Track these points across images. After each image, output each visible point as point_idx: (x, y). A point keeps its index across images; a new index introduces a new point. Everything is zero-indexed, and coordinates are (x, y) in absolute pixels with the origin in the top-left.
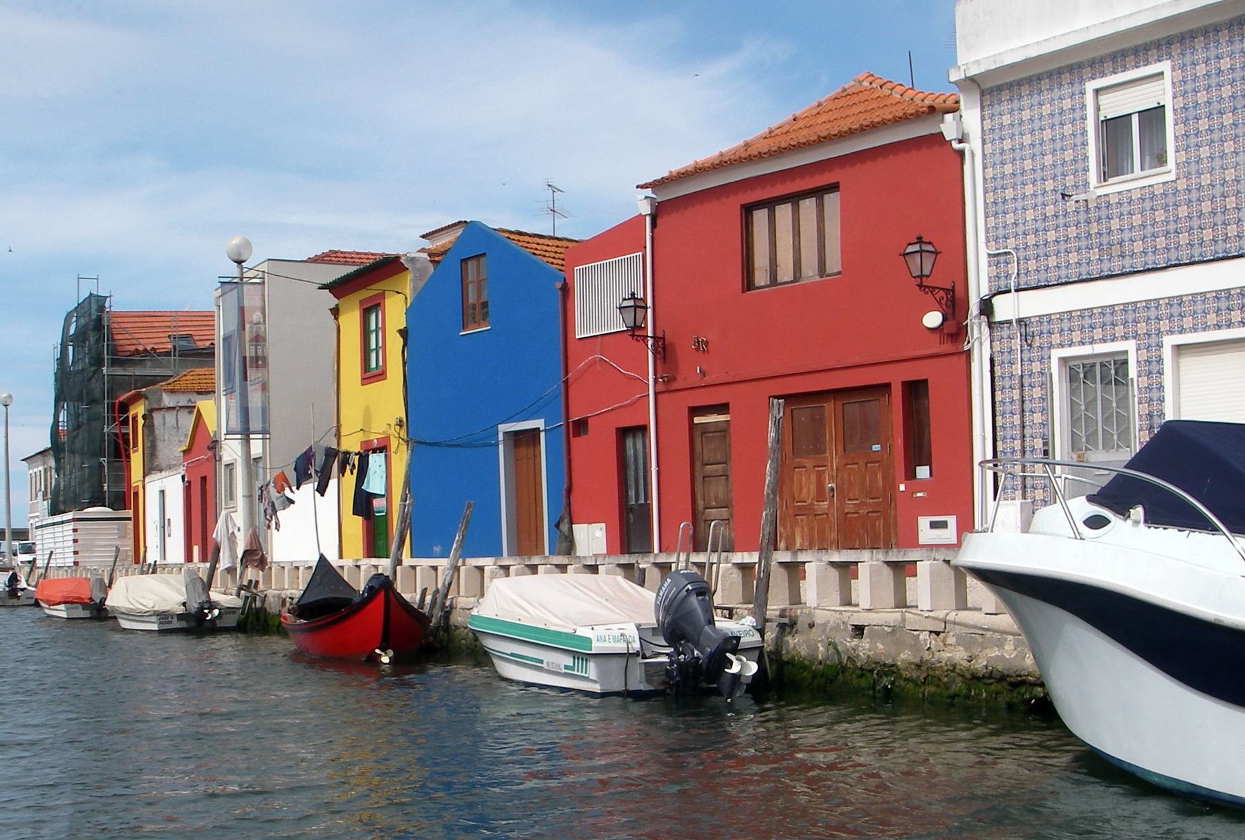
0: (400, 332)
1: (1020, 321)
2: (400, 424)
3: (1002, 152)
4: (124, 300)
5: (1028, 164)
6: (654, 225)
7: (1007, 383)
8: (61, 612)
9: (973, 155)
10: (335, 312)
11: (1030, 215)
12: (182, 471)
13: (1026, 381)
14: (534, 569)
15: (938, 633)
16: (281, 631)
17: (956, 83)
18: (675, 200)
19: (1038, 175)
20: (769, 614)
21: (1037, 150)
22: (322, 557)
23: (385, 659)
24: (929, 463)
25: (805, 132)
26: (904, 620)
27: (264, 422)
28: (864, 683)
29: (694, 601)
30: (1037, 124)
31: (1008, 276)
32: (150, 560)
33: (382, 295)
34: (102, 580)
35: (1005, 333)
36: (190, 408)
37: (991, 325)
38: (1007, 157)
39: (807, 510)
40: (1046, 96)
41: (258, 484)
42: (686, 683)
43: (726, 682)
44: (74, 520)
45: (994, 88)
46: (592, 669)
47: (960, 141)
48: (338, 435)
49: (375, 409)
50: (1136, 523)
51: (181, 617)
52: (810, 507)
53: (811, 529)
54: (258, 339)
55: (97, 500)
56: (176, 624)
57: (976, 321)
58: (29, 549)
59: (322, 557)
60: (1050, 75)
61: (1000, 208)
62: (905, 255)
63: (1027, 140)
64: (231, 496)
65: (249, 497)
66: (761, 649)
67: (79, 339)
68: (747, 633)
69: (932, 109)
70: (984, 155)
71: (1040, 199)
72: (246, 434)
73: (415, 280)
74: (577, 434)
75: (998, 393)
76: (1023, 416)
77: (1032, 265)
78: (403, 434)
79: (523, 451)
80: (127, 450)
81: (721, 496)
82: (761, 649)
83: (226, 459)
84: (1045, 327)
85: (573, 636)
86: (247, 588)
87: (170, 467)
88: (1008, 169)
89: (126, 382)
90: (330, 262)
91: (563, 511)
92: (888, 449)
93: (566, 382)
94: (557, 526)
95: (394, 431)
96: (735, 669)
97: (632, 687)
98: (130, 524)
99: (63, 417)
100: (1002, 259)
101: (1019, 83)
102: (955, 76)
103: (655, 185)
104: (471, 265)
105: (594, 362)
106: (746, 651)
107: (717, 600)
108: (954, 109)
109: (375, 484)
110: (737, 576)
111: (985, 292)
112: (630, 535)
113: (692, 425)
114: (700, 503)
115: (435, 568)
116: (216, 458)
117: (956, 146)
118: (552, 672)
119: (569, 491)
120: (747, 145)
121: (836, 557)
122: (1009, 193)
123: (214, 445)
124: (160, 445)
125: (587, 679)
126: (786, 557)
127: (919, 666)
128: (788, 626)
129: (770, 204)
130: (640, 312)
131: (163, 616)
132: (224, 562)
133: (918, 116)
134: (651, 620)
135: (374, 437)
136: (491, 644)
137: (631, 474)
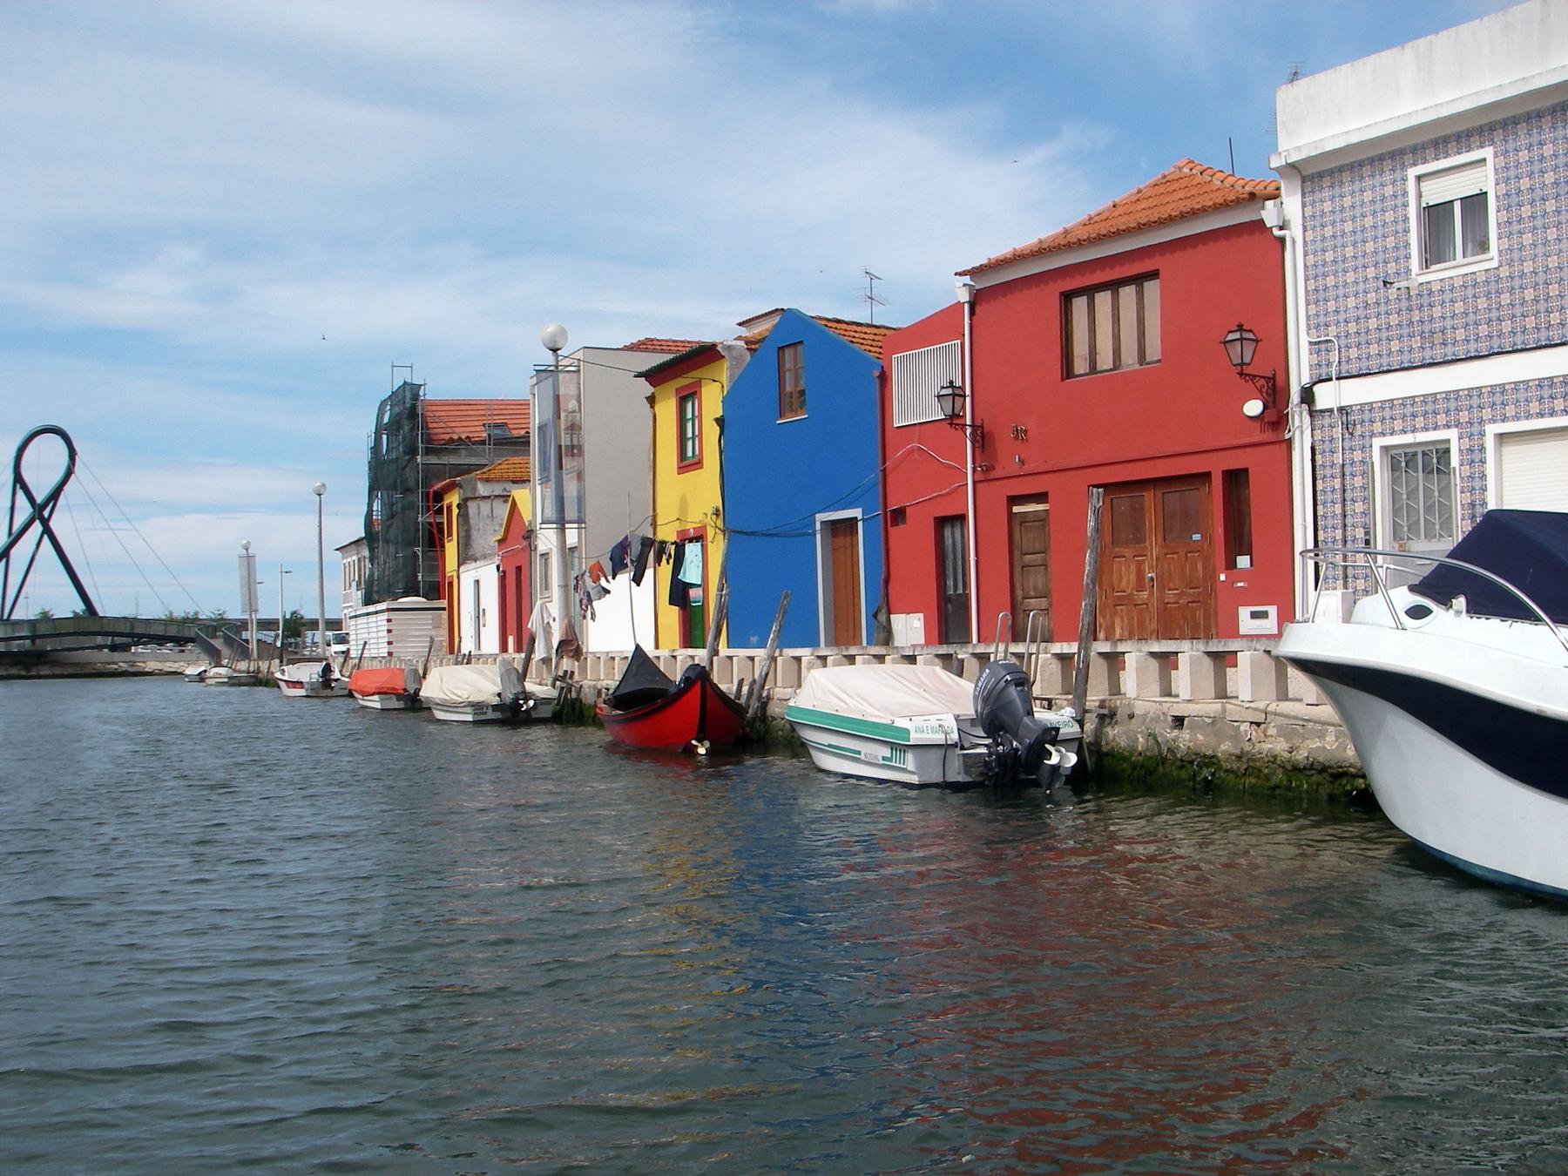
0: (718, 421)
1: (1341, 409)
2: (717, 513)
3: (1324, 239)
4: (441, 387)
5: (1349, 251)
6: (972, 313)
7: (1328, 472)
8: (375, 702)
9: (1294, 242)
10: (651, 400)
11: (1351, 302)
12: (497, 561)
13: (1348, 470)
14: (851, 659)
15: (1258, 724)
16: (597, 722)
17: (1277, 170)
18: (993, 288)
19: (1360, 262)
22: (638, 648)
23: (702, 751)
25: (1124, 219)
26: (1224, 711)
27: (579, 511)
30: (1358, 211)
31: (1329, 364)
32: (465, 651)
33: (698, 384)
34: (416, 671)
35: (1327, 421)
36: (505, 498)
37: (1312, 413)
38: (1329, 244)
39: (1126, 600)
41: (574, 574)
42: (1005, 774)
43: (1045, 772)
44: (388, 610)
45: (1315, 174)
46: (910, 761)
47: (1281, 228)
48: (654, 524)
50: (1459, 613)
51: (495, 708)
52: (1129, 597)
53: (1131, 619)
54: (574, 428)
55: (411, 590)
56: (491, 715)
58: (343, 640)
59: (638, 648)
61: (1321, 295)
62: (1225, 343)
63: (1348, 227)
64: (547, 586)
65: (565, 587)
67: (393, 427)
68: (1066, 724)
69: (1252, 196)
71: (1361, 287)
72: (561, 523)
73: (731, 368)
74: (895, 523)
75: (1319, 482)
76: (1344, 506)
77: (1354, 353)
78: (720, 523)
79: (841, 541)
80: (442, 540)
81: (1040, 585)
83: (541, 548)
84: (1367, 416)
85: (890, 727)
86: (563, 678)
87: (485, 557)
88: (1329, 256)
90: (646, 350)
91: (880, 601)
94: (875, 616)
96: (1054, 760)
97: (951, 778)
98: (445, 614)
99: (376, 506)
100: (1323, 347)
102: (1276, 162)
103: (974, 272)
104: (788, 353)
106: (1065, 742)
107: (1037, 690)
108: (1275, 196)
109: (691, 574)
110: (1056, 666)
111: (1306, 380)
112: (949, 625)
113: (1011, 514)
114: (1019, 593)
115: (752, 659)
116: (531, 548)
117: (1277, 232)
118: (870, 762)
119: (887, 581)
120: (1066, 232)
121: (1156, 647)
122: (1330, 281)
123: (529, 535)
124: (475, 534)
125: (905, 770)
126: (1103, 647)
127: (1239, 758)
128: (1108, 716)
129: (1090, 291)
131: (478, 707)
132: (540, 652)
134: (969, 710)
136: (809, 735)
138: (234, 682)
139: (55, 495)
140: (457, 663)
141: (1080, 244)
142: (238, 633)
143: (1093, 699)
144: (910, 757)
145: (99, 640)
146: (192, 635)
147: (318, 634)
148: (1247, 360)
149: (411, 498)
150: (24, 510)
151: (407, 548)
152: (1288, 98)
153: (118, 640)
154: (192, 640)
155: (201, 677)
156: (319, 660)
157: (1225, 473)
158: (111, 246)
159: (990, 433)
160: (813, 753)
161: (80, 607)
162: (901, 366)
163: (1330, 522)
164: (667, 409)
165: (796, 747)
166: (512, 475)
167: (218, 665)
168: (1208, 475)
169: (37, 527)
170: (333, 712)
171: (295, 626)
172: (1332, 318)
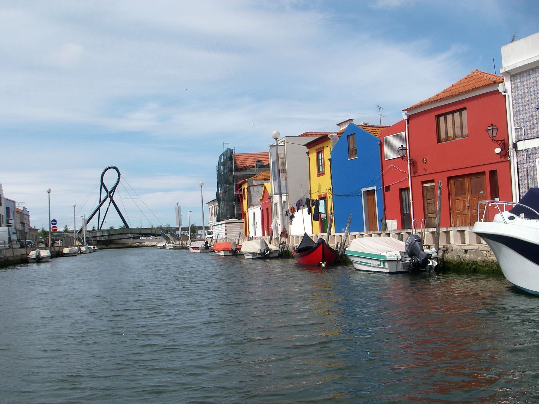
0: (329, 159)
1: (526, 150)
2: (330, 189)
3: (518, 95)
4: (240, 149)
5: (526, 99)
6: (408, 123)
7: (522, 170)
8: (222, 253)
9: (509, 96)
10: (308, 153)
11: (528, 115)
12: (260, 206)
13: (529, 169)
14: (371, 235)
15: (489, 251)
16: (293, 257)
17: (502, 73)
18: (415, 114)
19: (530, 102)
20: (440, 247)
21: (529, 94)
22: (305, 233)
23: (323, 265)
24: (498, 197)
25: (456, 90)
26: (479, 248)
27: (286, 190)
28: (468, 267)
29: (417, 243)
30: (529, 86)
31: (521, 135)
32: (251, 236)
33: (323, 148)
34: (235, 243)
35: (521, 154)
36: (262, 185)
37: (516, 151)
38: (520, 97)
39: (461, 213)
40: (531, 76)
41: (285, 210)
42: (415, 268)
43: (428, 268)
44: (225, 223)
45: (515, 74)
46: (387, 265)
47: (504, 92)
48: (310, 193)
49: (322, 185)
50: (522, 218)
51: (259, 254)
52: (461, 212)
53: (462, 219)
54: (283, 164)
55: (233, 216)
56: (258, 256)
57: (512, 150)
58: (210, 233)
59: (305, 233)
60: (532, 69)
61: (518, 113)
62: (487, 130)
63: (526, 91)
64: (277, 214)
65: (282, 214)
66: (437, 258)
67: (224, 163)
68: (433, 253)
69: (495, 82)
70: (512, 96)
71: (531, 110)
72: (280, 194)
73: (333, 143)
74: (386, 191)
75: (520, 173)
76: (528, 181)
77: (529, 131)
78: (331, 192)
79: (370, 197)
80: (242, 200)
81: (433, 209)
82: (437, 258)
83: (275, 202)
84: (534, 152)
85: (380, 256)
86: (282, 244)
87: (256, 205)
88: (520, 101)
89: (241, 177)
90: (306, 136)
91: (383, 216)
92: (485, 192)
93: (382, 174)
94: (381, 221)
95: (328, 192)
96: (431, 264)
97: (399, 270)
98: (244, 224)
99: (220, 189)
100: (519, 130)
101: (523, 72)
102: (502, 71)
103: (408, 110)
104: (351, 137)
105: (391, 168)
106: (433, 258)
107: (425, 243)
108: (502, 82)
109: (322, 209)
110: (431, 236)
111: (514, 141)
112: (405, 222)
113: (423, 187)
114: (426, 212)
115: (341, 236)
116: (271, 202)
117: (503, 94)
118: (374, 266)
119: (385, 209)
120: (437, 95)
121: (459, 229)
122: (521, 109)
123: (270, 198)
124: (253, 197)
125: (385, 268)
126: (445, 229)
127: (483, 262)
128: (446, 250)
129: (445, 115)
130: (405, 151)
131: (253, 254)
132: (275, 236)
133: (490, 85)
134: (404, 250)
135: (322, 194)
136: (352, 259)
137: (404, 203)
138: (175, 248)
139: (114, 189)
140: (248, 240)
141: (441, 100)
142: (175, 232)
143: (441, 245)
144: (386, 264)
145: (129, 235)
146: (160, 233)
147: (203, 231)
148: (494, 135)
149: (231, 186)
150: (104, 194)
151: (231, 201)
152: (506, 50)
153: (136, 235)
154: (160, 235)
155: (164, 247)
156: (203, 240)
157: (490, 171)
158: (129, 104)
159: (416, 161)
160: (355, 264)
161: (123, 224)
162: (386, 140)
163: (524, 186)
164: (313, 156)
165: (351, 263)
166: (264, 178)
167: (169, 243)
168: (485, 172)
169: (109, 199)
170: (208, 257)
171: (194, 229)
172: (522, 121)
